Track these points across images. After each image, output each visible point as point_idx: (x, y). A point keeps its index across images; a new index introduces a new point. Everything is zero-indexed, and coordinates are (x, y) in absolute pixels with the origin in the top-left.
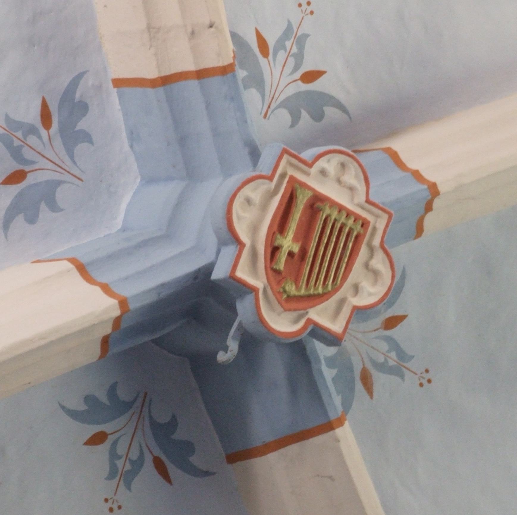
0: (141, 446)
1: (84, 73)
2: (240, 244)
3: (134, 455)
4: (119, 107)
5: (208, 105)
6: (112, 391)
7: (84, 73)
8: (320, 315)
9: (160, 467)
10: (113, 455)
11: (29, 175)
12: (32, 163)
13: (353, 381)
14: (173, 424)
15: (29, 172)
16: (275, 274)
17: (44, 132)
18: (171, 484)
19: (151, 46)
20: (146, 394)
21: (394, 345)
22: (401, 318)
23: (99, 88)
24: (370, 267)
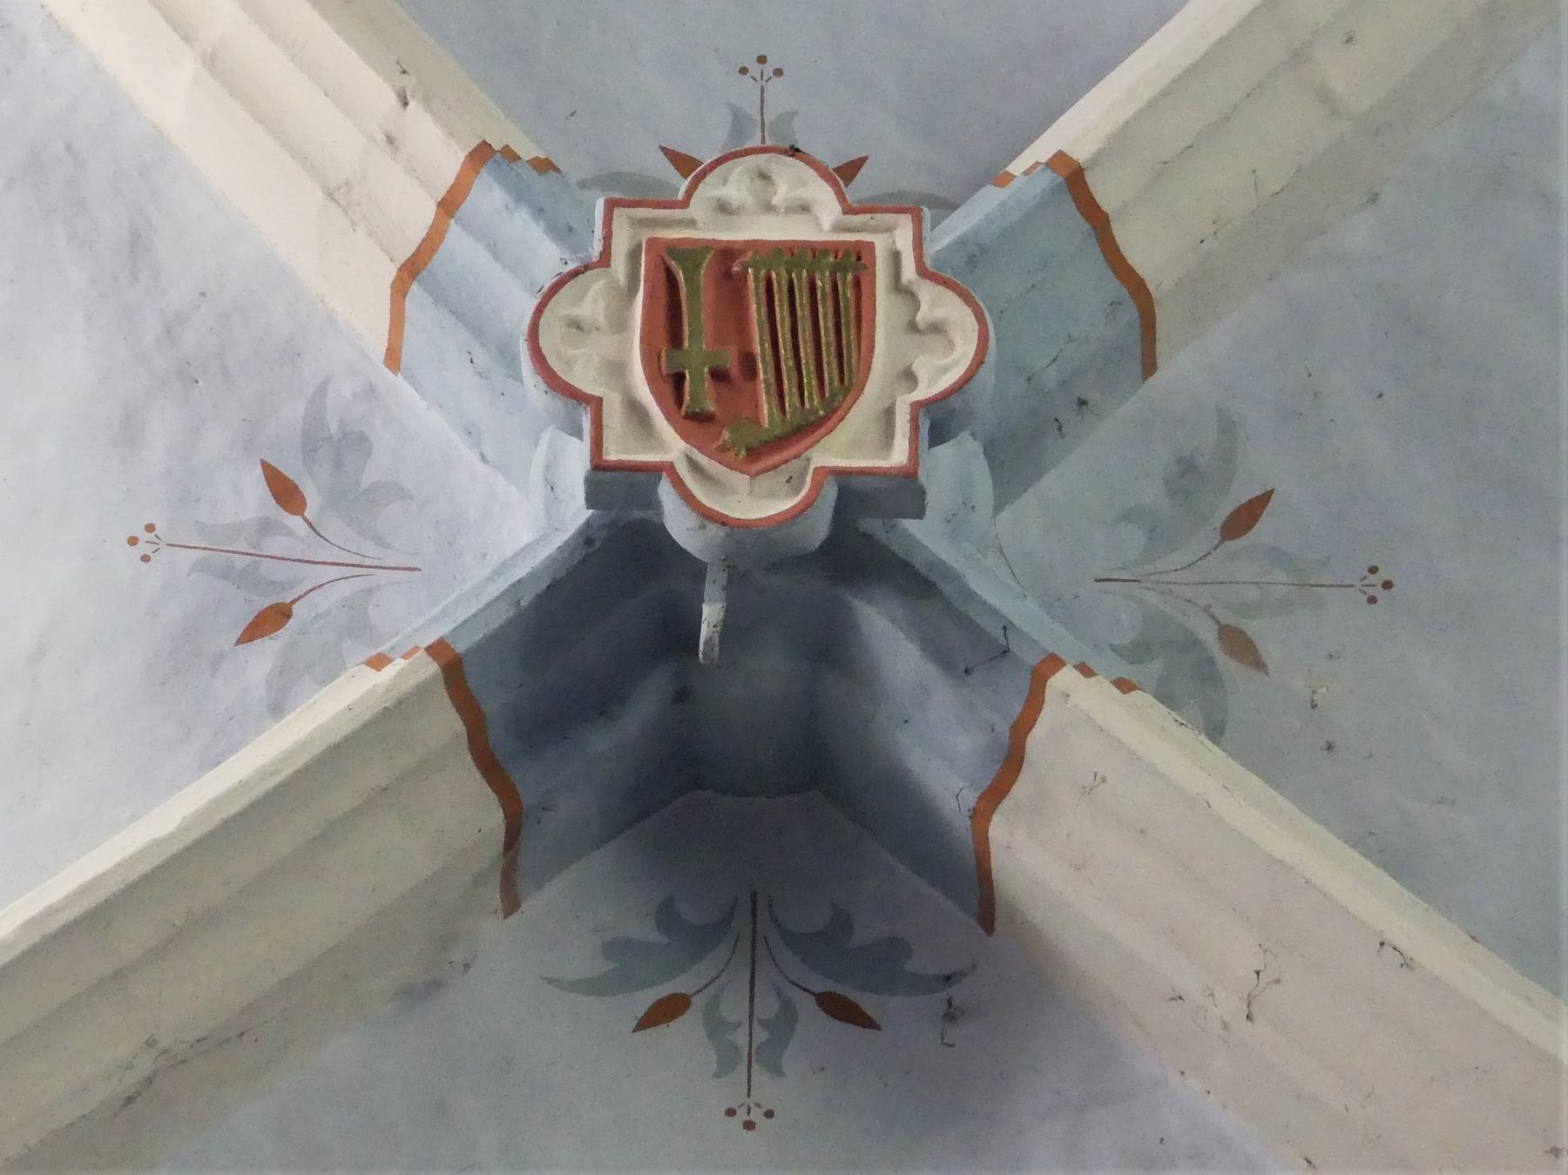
0: (777, 989)
1: (326, 382)
2: (596, 404)
3: (768, 1006)
4: (425, 404)
5: (494, 250)
6: (666, 915)
7: (326, 382)
8: (845, 448)
9: (838, 1008)
10: (716, 1027)
11: (295, 607)
12: (293, 584)
13: (1211, 661)
14: (843, 921)
15: (294, 602)
16: (695, 421)
17: (293, 522)
18: (878, 1028)
19: (353, 223)
20: (754, 895)
21: (1276, 555)
22: (1263, 500)
23: (371, 391)
24: (921, 326)
